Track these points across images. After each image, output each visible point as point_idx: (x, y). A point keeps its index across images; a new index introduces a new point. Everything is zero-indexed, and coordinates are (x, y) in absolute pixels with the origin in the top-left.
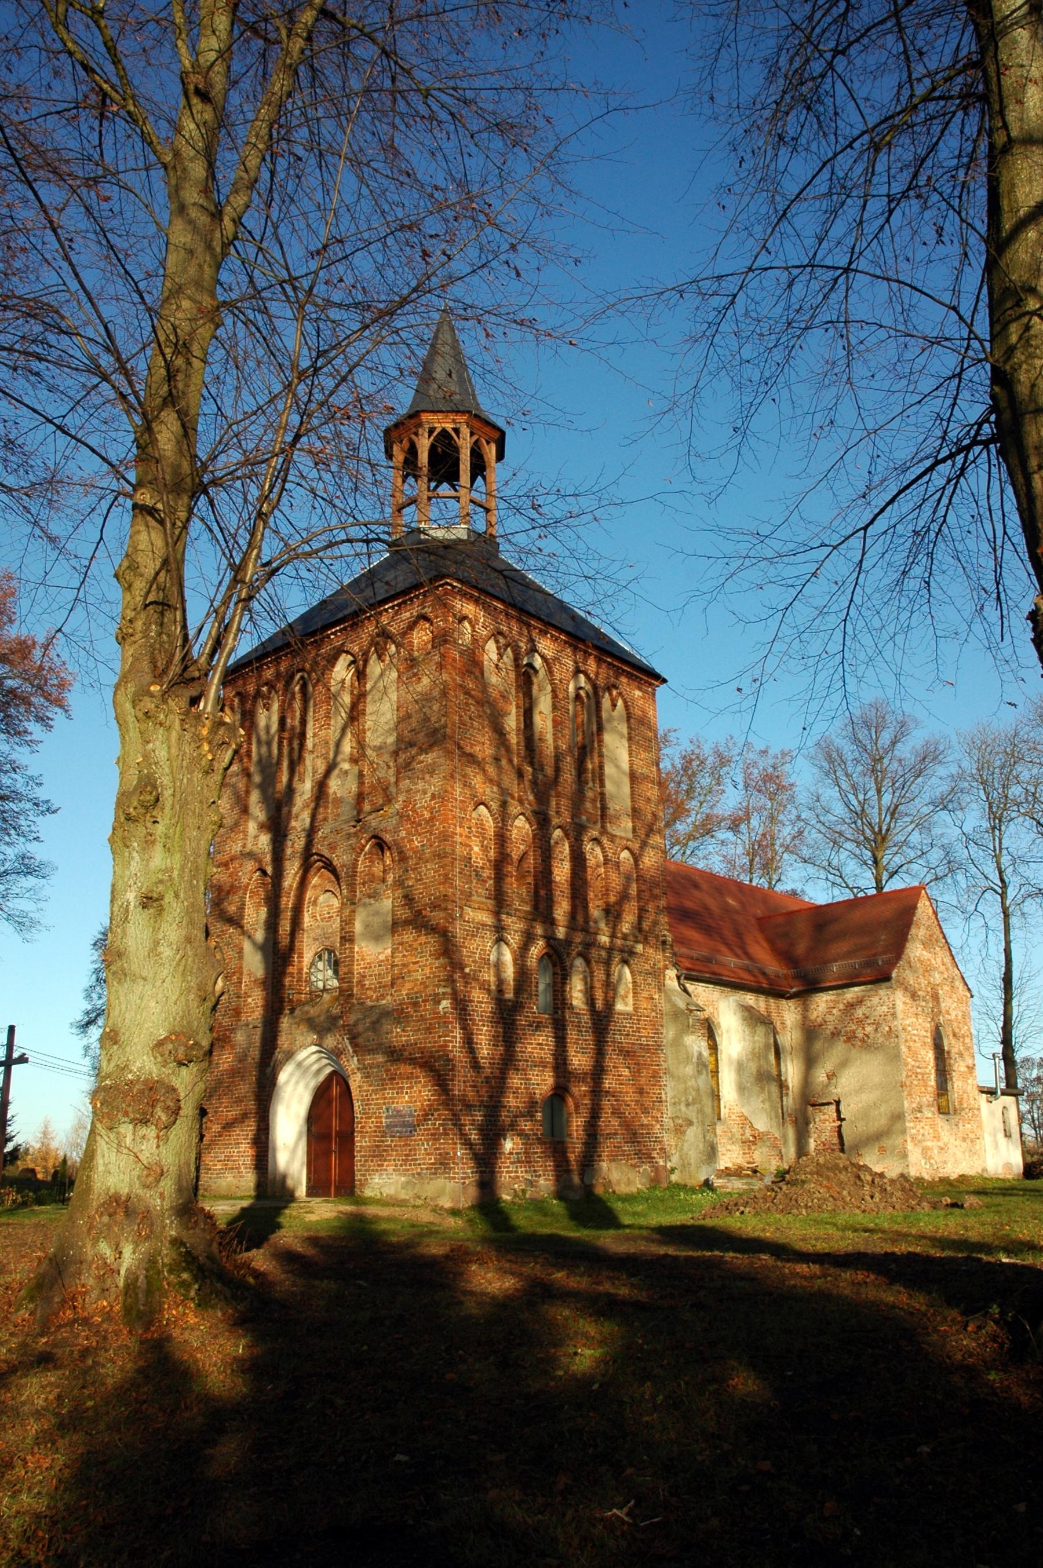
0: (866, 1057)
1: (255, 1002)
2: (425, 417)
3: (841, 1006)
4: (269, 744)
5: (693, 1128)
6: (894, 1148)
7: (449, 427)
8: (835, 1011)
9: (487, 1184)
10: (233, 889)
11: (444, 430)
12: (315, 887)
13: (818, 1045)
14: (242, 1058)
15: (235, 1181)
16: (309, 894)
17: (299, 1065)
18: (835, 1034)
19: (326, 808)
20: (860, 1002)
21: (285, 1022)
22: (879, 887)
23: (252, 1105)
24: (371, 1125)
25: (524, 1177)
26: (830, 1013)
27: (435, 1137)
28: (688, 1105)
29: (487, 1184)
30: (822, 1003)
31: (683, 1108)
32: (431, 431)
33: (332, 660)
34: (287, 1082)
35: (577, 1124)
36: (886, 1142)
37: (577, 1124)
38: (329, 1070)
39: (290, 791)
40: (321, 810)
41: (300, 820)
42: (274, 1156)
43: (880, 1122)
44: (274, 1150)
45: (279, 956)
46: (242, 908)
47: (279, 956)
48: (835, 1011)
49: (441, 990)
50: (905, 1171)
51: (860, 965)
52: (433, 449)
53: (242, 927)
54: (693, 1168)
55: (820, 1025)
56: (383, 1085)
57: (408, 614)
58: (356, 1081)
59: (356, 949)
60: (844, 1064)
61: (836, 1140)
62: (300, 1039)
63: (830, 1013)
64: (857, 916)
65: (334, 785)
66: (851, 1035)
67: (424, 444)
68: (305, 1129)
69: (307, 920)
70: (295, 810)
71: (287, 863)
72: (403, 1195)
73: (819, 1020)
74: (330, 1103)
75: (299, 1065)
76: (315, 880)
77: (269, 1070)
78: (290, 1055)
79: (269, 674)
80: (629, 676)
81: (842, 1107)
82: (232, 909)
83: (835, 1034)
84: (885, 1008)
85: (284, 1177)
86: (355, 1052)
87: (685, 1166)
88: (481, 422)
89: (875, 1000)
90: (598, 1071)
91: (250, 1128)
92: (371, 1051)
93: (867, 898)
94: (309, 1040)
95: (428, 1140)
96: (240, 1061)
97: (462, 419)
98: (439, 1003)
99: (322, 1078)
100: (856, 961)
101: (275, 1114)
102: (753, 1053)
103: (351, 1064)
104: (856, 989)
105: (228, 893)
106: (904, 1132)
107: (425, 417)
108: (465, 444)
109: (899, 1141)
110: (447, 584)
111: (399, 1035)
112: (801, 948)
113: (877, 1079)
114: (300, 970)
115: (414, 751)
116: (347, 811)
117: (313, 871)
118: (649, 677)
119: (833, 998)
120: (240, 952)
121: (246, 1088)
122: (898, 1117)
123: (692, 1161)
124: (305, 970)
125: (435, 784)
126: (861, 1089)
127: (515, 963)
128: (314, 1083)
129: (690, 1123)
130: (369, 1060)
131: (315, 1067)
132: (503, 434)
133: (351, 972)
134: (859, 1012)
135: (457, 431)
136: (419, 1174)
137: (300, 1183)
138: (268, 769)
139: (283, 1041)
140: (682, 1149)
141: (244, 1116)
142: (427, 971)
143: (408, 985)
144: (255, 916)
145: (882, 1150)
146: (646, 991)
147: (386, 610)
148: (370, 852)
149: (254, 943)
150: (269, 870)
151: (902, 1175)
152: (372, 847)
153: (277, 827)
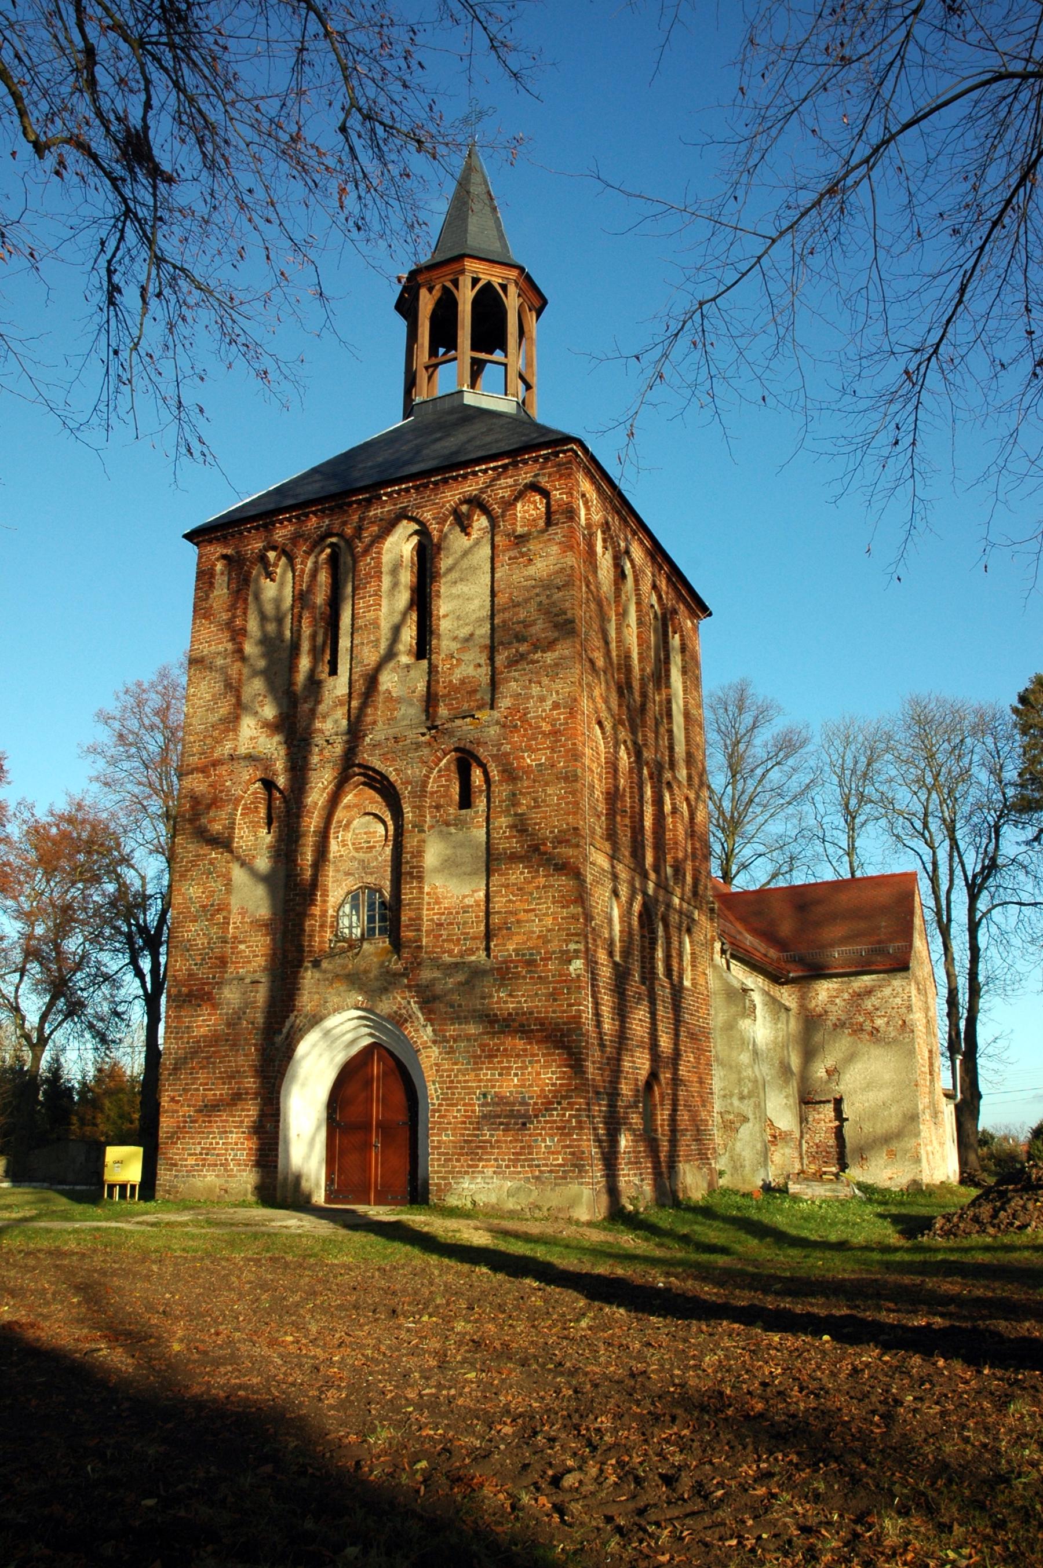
0: (876, 1051)
1: (254, 953)
2: (470, 265)
3: (846, 996)
4: (280, 620)
5: (748, 1125)
6: (906, 1152)
7: (496, 281)
8: (837, 1001)
9: (613, 1191)
10: (215, 802)
11: (489, 284)
12: (348, 807)
13: (818, 1038)
14: (233, 1022)
15: (218, 1182)
16: (340, 814)
17: (327, 1033)
18: (840, 1025)
19: (376, 709)
20: (869, 992)
21: (309, 978)
22: (853, 873)
23: (250, 1083)
24: (456, 1114)
25: (636, 1185)
26: (832, 1003)
27: (564, 1130)
28: (742, 1098)
29: (613, 1191)
30: (824, 991)
31: (736, 1102)
32: (475, 281)
33: (388, 527)
34: (308, 1054)
35: (662, 1115)
36: (895, 1145)
37: (662, 1115)
38: (367, 1041)
39: (314, 684)
40: (369, 711)
41: (330, 724)
42: (287, 1151)
43: (892, 1121)
44: (287, 1143)
45: (293, 892)
46: (232, 827)
47: (293, 892)
48: (837, 1001)
49: (572, 947)
50: (918, 1178)
51: (868, 952)
52: (475, 302)
53: (231, 852)
54: (748, 1169)
55: (821, 1015)
56: (476, 1061)
57: (510, 481)
58: (431, 1060)
59: (426, 889)
60: (851, 1058)
61: (832, 1142)
62: (334, 1000)
63: (832, 1003)
64: (844, 899)
65: (388, 681)
66: (859, 1026)
67: (466, 296)
68: (324, 1115)
69: (334, 846)
70: (322, 708)
71: (313, 776)
72: (511, 1205)
73: (819, 1009)
74: (368, 1083)
75: (327, 1033)
76: (348, 799)
77: (279, 1039)
78: (316, 1020)
79: (281, 533)
80: (688, 606)
81: (845, 1107)
82: (217, 827)
83: (840, 1025)
84: (898, 1000)
85: (298, 1178)
86: (427, 1019)
87: (737, 1166)
88: (529, 286)
89: (887, 991)
90: (677, 1055)
91: (250, 1112)
92: (458, 1018)
93: (844, 881)
94: (350, 1001)
95: (552, 1136)
96: (229, 1025)
97: (513, 274)
98: (569, 962)
99: (355, 1050)
100: (862, 948)
101: (288, 1094)
102: (776, 1043)
103: (421, 1033)
104: (866, 978)
105: (209, 807)
106: (918, 1134)
107: (470, 265)
108: (512, 302)
109: (912, 1143)
110: (572, 450)
111: (504, 1001)
112: (786, 929)
113: (887, 1077)
114: (324, 913)
115: (523, 648)
116: (411, 712)
117: (348, 787)
118: (700, 608)
119: (836, 986)
120: (228, 884)
121: (246, 1058)
122: (913, 1118)
123: (747, 1163)
124: (331, 912)
125: (559, 689)
126: (869, 1086)
127: (621, 921)
128: (341, 1057)
129: (745, 1119)
130: (451, 1030)
131: (349, 1036)
132: (545, 302)
133: (419, 918)
134: (869, 1004)
135: (504, 287)
136: (537, 1178)
137: (318, 1185)
138: (280, 656)
139: (307, 1001)
140: (733, 1149)
141: (236, 1098)
142: (549, 922)
143: (517, 939)
144: (255, 839)
145: (892, 1154)
146: (711, 969)
147: (475, 474)
148: (447, 768)
149: (253, 873)
150: (281, 781)
151: (915, 1182)
152: (449, 762)
153: (294, 728)
